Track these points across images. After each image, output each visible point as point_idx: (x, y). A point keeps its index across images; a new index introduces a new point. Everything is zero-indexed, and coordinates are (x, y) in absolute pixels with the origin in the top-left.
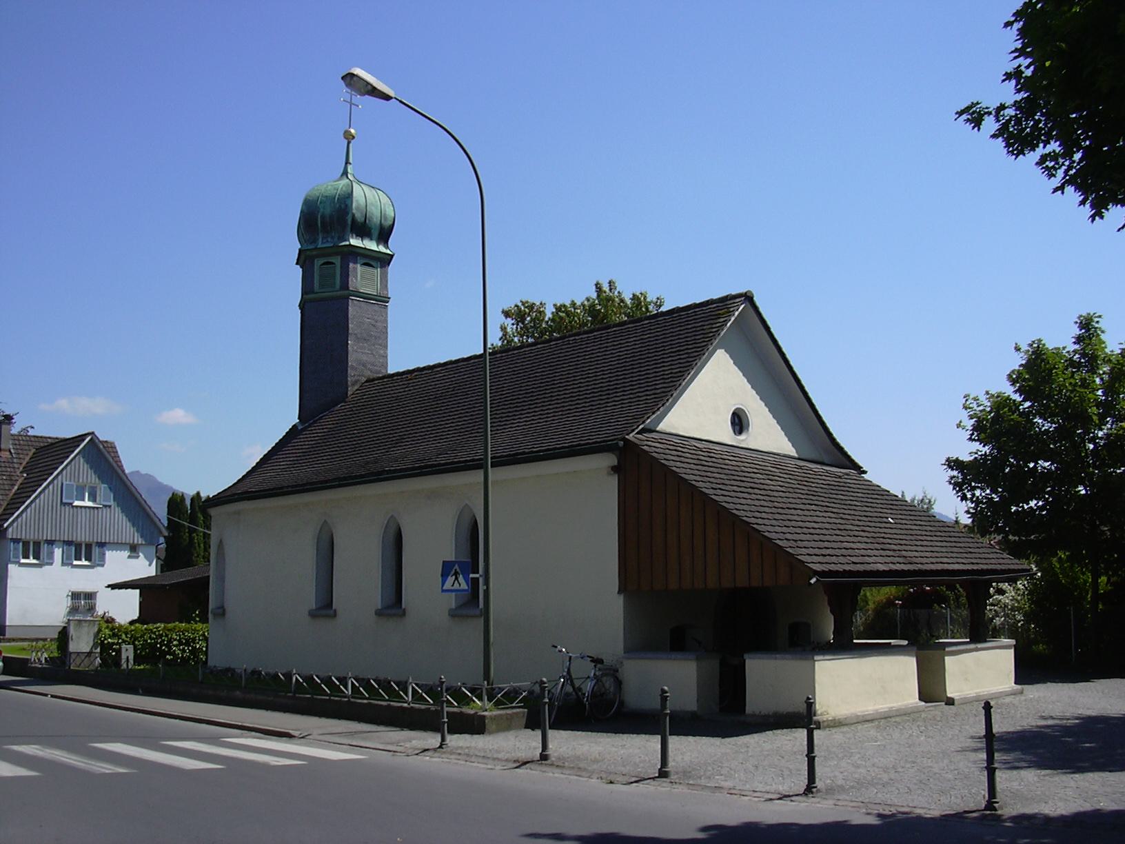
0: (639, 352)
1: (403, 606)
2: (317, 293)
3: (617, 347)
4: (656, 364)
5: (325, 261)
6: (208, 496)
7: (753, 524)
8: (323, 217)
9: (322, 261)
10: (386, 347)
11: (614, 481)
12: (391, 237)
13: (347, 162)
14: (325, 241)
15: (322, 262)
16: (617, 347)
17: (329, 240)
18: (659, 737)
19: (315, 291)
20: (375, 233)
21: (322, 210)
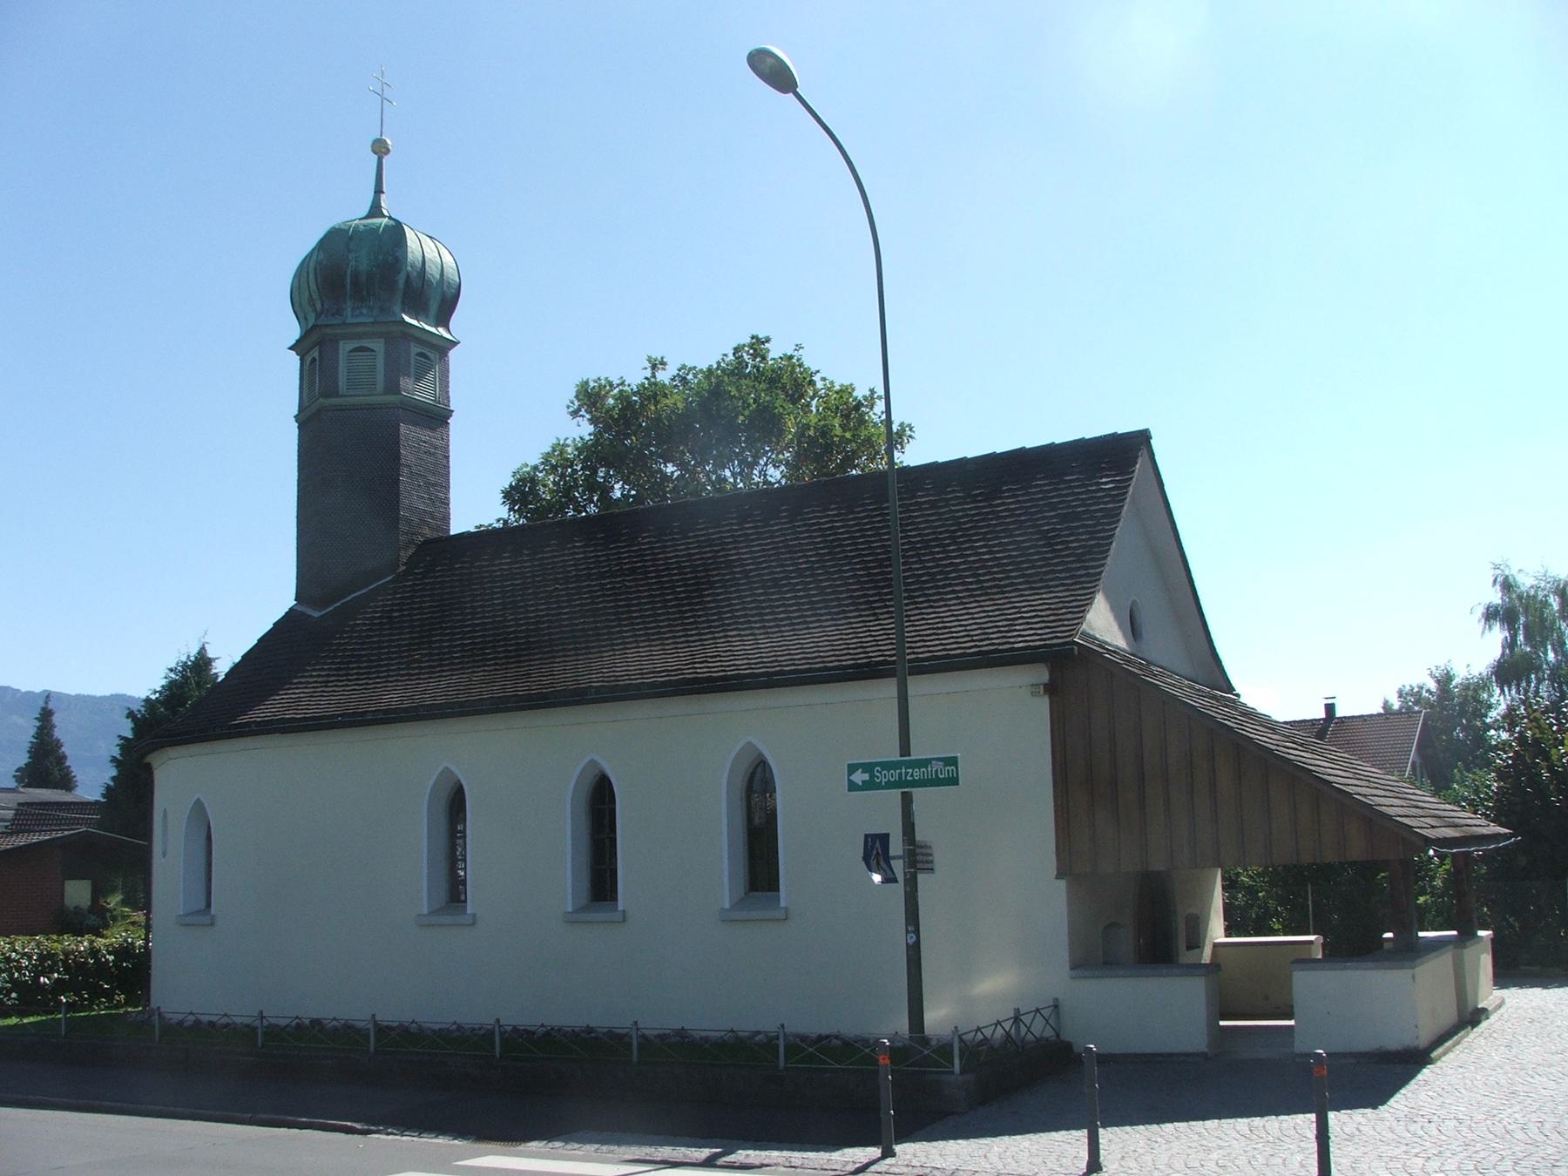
0: (479, 688)
1: (212, 913)
2: (341, 396)
3: (414, 682)
4: (628, 666)
5: (358, 345)
6: (202, 663)
7: (1416, 828)
8: (356, 275)
9: (351, 345)
10: (447, 488)
11: (1043, 704)
12: (818, 114)
13: (379, 191)
14: (357, 312)
15: (352, 347)
16: (414, 682)
17: (365, 311)
18: (1085, 1132)
19: (340, 393)
20: (434, 306)
21: (353, 263)
